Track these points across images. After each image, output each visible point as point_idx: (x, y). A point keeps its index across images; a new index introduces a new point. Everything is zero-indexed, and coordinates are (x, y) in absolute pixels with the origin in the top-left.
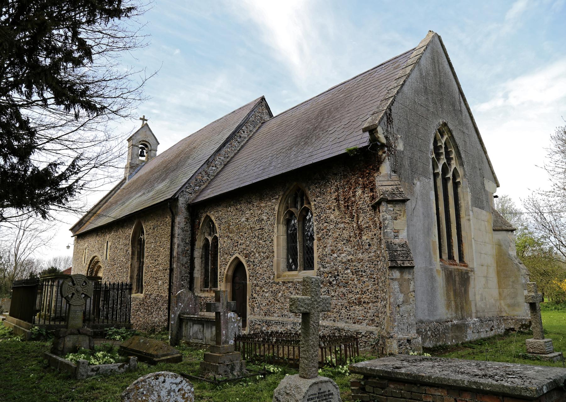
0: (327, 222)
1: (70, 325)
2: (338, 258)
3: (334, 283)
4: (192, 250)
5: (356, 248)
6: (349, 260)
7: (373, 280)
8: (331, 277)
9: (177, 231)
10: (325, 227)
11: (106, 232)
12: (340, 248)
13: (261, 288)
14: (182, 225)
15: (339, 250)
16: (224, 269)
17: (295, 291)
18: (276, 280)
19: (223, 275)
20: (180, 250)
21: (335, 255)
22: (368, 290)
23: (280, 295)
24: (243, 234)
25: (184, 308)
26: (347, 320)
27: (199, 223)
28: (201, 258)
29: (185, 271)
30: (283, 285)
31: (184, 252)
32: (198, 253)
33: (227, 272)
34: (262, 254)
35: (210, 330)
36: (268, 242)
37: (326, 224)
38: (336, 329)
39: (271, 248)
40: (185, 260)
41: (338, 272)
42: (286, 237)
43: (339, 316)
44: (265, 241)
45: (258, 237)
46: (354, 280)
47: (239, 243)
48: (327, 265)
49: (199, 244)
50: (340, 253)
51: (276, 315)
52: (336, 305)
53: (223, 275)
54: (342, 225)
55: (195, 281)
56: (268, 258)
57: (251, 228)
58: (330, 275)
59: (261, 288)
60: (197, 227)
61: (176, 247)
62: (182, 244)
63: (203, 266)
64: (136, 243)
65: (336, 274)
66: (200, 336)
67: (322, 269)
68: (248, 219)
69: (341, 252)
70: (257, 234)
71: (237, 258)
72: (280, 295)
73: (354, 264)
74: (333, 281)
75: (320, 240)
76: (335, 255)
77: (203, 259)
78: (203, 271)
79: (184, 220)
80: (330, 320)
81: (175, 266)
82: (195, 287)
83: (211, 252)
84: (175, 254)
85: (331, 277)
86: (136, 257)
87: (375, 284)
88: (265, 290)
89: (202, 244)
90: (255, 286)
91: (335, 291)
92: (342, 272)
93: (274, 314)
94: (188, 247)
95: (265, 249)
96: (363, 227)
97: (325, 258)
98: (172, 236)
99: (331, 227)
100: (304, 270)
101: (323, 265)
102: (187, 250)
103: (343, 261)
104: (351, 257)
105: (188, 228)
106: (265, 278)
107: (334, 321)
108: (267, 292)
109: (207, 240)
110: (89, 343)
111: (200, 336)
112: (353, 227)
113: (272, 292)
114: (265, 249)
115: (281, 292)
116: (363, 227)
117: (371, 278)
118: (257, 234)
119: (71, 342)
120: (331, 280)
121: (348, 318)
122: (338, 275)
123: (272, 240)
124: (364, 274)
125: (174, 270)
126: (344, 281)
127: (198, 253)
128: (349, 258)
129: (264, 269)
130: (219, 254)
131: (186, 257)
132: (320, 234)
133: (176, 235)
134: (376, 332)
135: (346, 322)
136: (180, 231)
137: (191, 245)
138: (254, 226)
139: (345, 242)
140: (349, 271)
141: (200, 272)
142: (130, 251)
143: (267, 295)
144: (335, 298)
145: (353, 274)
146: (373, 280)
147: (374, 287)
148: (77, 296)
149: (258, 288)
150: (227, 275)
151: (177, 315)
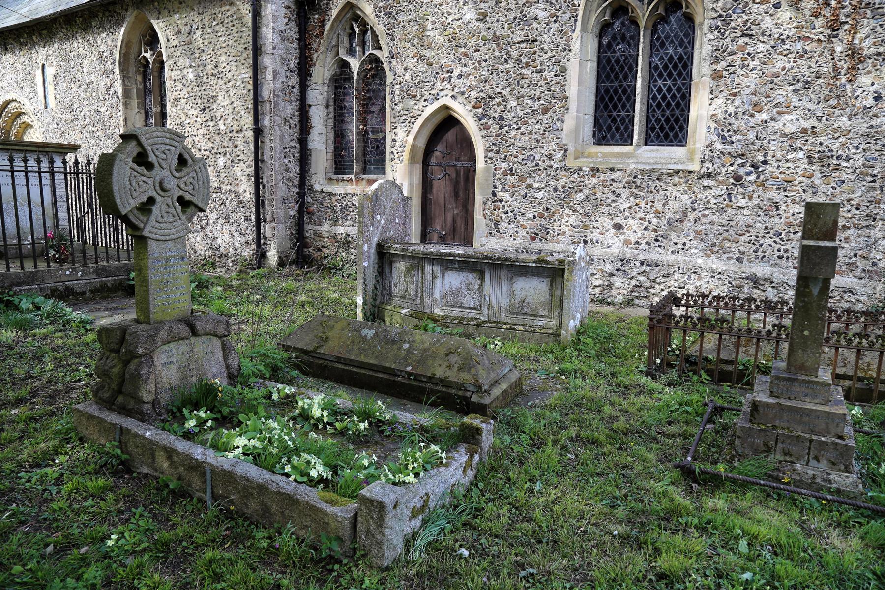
0: (751, 36)
1: (156, 313)
2: (772, 123)
3: (752, 178)
4: (304, 87)
5: (833, 102)
6: (804, 131)
7: (870, 179)
8: (742, 165)
9: (269, 35)
10: (742, 48)
11: (34, 44)
12: (782, 100)
13: (522, 178)
14: (281, 24)
15: (776, 106)
16: (403, 138)
17: (628, 191)
18: (572, 163)
19: (402, 146)
20: (279, 85)
21: (764, 116)
22: (849, 200)
23: (580, 196)
24: (470, 52)
25: (386, 227)
26: (779, 261)
27: (323, 23)
28: (327, 106)
29: (291, 135)
30: (593, 176)
31: (287, 89)
32: (319, 95)
33: (415, 139)
34: (530, 102)
35: (505, 287)
36: (549, 75)
37: (746, 40)
38: (747, 278)
39: (558, 88)
40: (290, 109)
41: (766, 155)
42: (595, 64)
43: (756, 251)
44: (540, 72)
45: (519, 61)
46: (812, 176)
47: (456, 73)
48: (733, 139)
49: (322, 72)
50: (780, 113)
51: (568, 240)
52: (749, 226)
53: (402, 146)
54: (799, 46)
55: (313, 159)
56: (545, 111)
57: (496, 38)
58: (740, 161)
59: (522, 178)
60: (316, 32)
61: (269, 76)
62: (282, 70)
63: (331, 124)
64: (132, 69)
65: (761, 159)
66: (469, 301)
67: (719, 146)
68: (485, 15)
69: (784, 109)
70: (515, 54)
71: (446, 108)
72: (580, 196)
73: (820, 139)
74: (748, 174)
75: (721, 77)
76: (764, 116)
77: (332, 108)
78: (332, 135)
79: (283, 11)
80: (729, 258)
81: (266, 122)
82: (313, 170)
83: (364, 92)
84: (265, 93)
85: (742, 165)
86: (135, 102)
87: (875, 189)
88: (536, 185)
89: (328, 75)
90: (505, 173)
91: (751, 198)
92: (778, 156)
93: (561, 238)
94: (294, 80)
95: (539, 90)
96: (865, 52)
97: (732, 121)
98: (257, 50)
99: (761, 47)
100: (646, 144)
101: (724, 137)
102: (293, 87)
103: (787, 131)
104: (813, 122)
105: (293, 33)
106: (538, 157)
107: (739, 260)
108: (540, 189)
109: (344, 65)
110: (226, 358)
111: (469, 301)
112: (833, 51)
113: (556, 189)
114: (539, 90)
115: (586, 191)
116: (865, 52)
117: (866, 175)
118: (515, 54)
119: (174, 367)
120: (742, 172)
121: (780, 257)
122: (765, 162)
123: (564, 70)
124: (844, 164)
125: (266, 132)
126: (781, 176)
127: (319, 95)
128: (807, 124)
129: (534, 136)
130: (389, 98)
131: (291, 102)
132: (723, 64)
133: (268, 48)
134: (860, 290)
135: (776, 265)
136: (277, 39)
137: (300, 75)
138: (505, 32)
139: (798, 86)
140: (801, 154)
141: (324, 137)
142: (119, 87)
143: (540, 195)
144: (746, 212)
145: (811, 163)
146: (870, 179)
147: (868, 195)
148: (164, 207)
149: (511, 180)
150: (413, 147)
151: (374, 245)
